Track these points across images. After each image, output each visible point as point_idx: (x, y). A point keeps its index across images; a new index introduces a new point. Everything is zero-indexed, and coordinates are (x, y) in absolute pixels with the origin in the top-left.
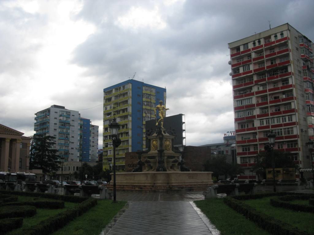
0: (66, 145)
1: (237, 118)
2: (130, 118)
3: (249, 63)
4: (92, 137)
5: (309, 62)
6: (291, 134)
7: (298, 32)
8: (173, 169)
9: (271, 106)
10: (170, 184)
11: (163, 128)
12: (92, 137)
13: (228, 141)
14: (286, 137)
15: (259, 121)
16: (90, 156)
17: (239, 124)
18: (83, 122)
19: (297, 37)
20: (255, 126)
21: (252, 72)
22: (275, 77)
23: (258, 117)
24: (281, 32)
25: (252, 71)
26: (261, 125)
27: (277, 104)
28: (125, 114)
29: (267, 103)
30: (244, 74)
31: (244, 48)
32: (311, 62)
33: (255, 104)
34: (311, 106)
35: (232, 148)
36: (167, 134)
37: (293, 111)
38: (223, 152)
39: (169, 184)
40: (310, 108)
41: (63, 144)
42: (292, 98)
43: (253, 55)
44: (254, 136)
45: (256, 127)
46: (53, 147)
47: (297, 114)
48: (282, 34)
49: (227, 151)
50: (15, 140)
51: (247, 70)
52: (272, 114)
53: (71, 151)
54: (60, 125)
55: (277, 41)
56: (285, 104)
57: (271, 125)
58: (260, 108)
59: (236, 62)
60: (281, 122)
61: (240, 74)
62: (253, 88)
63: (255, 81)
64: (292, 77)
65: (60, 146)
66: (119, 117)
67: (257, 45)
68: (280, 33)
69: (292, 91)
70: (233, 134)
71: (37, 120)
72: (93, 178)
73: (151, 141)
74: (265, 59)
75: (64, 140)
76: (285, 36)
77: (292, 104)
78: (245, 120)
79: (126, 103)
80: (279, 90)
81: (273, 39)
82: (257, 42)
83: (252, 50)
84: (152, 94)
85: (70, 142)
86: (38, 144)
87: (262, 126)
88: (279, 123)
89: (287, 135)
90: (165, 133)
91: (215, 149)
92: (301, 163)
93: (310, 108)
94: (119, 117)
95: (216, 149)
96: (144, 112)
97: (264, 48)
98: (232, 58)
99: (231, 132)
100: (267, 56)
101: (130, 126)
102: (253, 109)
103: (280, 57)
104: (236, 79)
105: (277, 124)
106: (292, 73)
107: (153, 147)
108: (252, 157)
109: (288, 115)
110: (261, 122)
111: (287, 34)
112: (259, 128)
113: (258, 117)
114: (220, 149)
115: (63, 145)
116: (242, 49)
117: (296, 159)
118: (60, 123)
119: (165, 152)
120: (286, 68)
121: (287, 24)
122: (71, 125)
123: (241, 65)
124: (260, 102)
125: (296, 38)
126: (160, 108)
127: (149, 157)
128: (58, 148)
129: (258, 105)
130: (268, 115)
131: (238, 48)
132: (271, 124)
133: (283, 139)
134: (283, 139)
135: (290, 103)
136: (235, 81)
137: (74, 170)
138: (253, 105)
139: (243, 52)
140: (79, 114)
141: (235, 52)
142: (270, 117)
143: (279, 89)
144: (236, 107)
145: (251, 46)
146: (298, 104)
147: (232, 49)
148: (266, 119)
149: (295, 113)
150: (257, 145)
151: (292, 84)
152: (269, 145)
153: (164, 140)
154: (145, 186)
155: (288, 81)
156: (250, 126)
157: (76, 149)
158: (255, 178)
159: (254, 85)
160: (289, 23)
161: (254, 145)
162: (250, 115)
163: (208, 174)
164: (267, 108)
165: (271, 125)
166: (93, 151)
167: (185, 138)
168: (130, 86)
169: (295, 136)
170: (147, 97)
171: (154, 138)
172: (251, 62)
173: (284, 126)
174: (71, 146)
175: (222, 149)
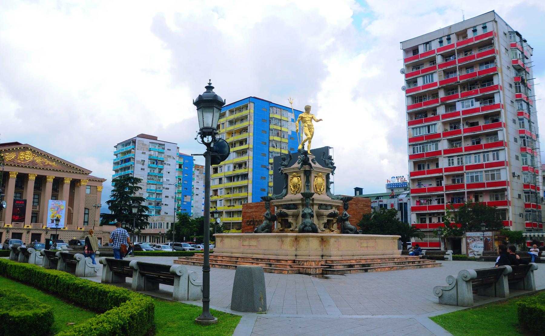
0: (157, 192)
1: (412, 154)
2: (251, 153)
3: (432, 72)
4: (195, 181)
5: (524, 72)
6: (496, 180)
7: (507, 25)
8: (329, 229)
9: (466, 138)
10: (328, 258)
11: (311, 154)
12: (195, 181)
13: (392, 190)
14: (489, 185)
15: (447, 160)
17: (415, 163)
18: (184, 161)
19: (506, 32)
20: (440, 167)
21: (437, 85)
22: (473, 92)
23: (444, 154)
24: (483, 24)
25: (436, 83)
27: (475, 133)
28: (244, 147)
29: (460, 132)
30: (424, 87)
32: (527, 72)
33: (440, 134)
34: (527, 138)
35: (400, 200)
36: (318, 165)
37: (501, 144)
38: (386, 205)
39: (325, 258)
40: (524, 140)
41: (153, 190)
42: (500, 125)
43: (439, 60)
44: (437, 182)
46: (137, 194)
47: (506, 148)
48: (485, 28)
49: (392, 205)
50: (79, 181)
51: (429, 81)
52: (467, 149)
53: (164, 201)
54: (150, 163)
55: (477, 38)
56: (488, 135)
57: (466, 166)
59: (410, 71)
60: (482, 162)
61: (419, 89)
62: (437, 108)
63: (441, 99)
64: (499, 92)
65: (149, 192)
66: (234, 152)
67: (445, 43)
68: (482, 26)
69: (498, 114)
70: (399, 180)
71: (116, 155)
72: (195, 240)
73: (290, 177)
74: (458, 65)
75: (156, 184)
76: (489, 30)
77: (499, 133)
78: (425, 158)
79: (244, 131)
80: (479, 111)
81: (470, 35)
82: (445, 39)
83: (437, 52)
84: (283, 118)
85: (164, 188)
87: (451, 166)
88: (477, 163)
89: (490, 181)
90: (315, 163)
91: (374, 202)
92: (511, 225)
93: (524, 140)
95: (376, 202)
96: (271, 145)
97: (456, 48)
98: (406, 63)
99: (397, 177)
100: (460, 61)
101: (250, 165)
102: (438, 141)
103: (481, 63)
104: (412, 96)
105: (476, 164)
106: (499, 87)
107: (292, 187)
108: (434, 214)
109: (493, 151)
110: (449, 160)
111: (493, 26)
112: (447, 170)
113: (444, 154)
114: (382, 201)
115: (154, 192)
116: (421, 50)
117: (504, 218)
118: (150, 161)
119: (315, 196)
120: (490, 79)
121: (493, 11)
122: (165, 164)
123: (420, 75)
124: (449, 130)
125: (505, 34)
126: (307, 119)
127: (288, 207)
128: (146, 195)
129: (445, 134)
130: (460, 150)
131: (415, 50)
132: (465, 165)
134: (484, 187)
135: (496, 133)
136: (410, 99)
137: (167, 228)
138: (438, 135)
139: (422, 55)
140: (178, 148)
141: (411, 55)
142: (464, 153)
144: (411, 137)
145: (435, 46)
146: (508, 133)
147: (406, 51)
148: (458, 156)
149: (503, 148)
150: (442, 195)
151: (499, 103)
152: (291, 229)
153: (313, 175)
154: (278, 260)
155: (493, 99)
156: (433, 167)
158: (440, 246)
159: (440, 105)
160: (495, 11)
161: (439, 196)
163: (393, 238)
164: (460, 139)
165: (466, 166)
166: (197, 202)
167: (333, 183)
168: (251, 109)
169: (504, 183)
170: (276, 123)
171: (295, 172)
172: (436, 70)
173: (486, 168)
174: (165, 193)
175: (385, 201)
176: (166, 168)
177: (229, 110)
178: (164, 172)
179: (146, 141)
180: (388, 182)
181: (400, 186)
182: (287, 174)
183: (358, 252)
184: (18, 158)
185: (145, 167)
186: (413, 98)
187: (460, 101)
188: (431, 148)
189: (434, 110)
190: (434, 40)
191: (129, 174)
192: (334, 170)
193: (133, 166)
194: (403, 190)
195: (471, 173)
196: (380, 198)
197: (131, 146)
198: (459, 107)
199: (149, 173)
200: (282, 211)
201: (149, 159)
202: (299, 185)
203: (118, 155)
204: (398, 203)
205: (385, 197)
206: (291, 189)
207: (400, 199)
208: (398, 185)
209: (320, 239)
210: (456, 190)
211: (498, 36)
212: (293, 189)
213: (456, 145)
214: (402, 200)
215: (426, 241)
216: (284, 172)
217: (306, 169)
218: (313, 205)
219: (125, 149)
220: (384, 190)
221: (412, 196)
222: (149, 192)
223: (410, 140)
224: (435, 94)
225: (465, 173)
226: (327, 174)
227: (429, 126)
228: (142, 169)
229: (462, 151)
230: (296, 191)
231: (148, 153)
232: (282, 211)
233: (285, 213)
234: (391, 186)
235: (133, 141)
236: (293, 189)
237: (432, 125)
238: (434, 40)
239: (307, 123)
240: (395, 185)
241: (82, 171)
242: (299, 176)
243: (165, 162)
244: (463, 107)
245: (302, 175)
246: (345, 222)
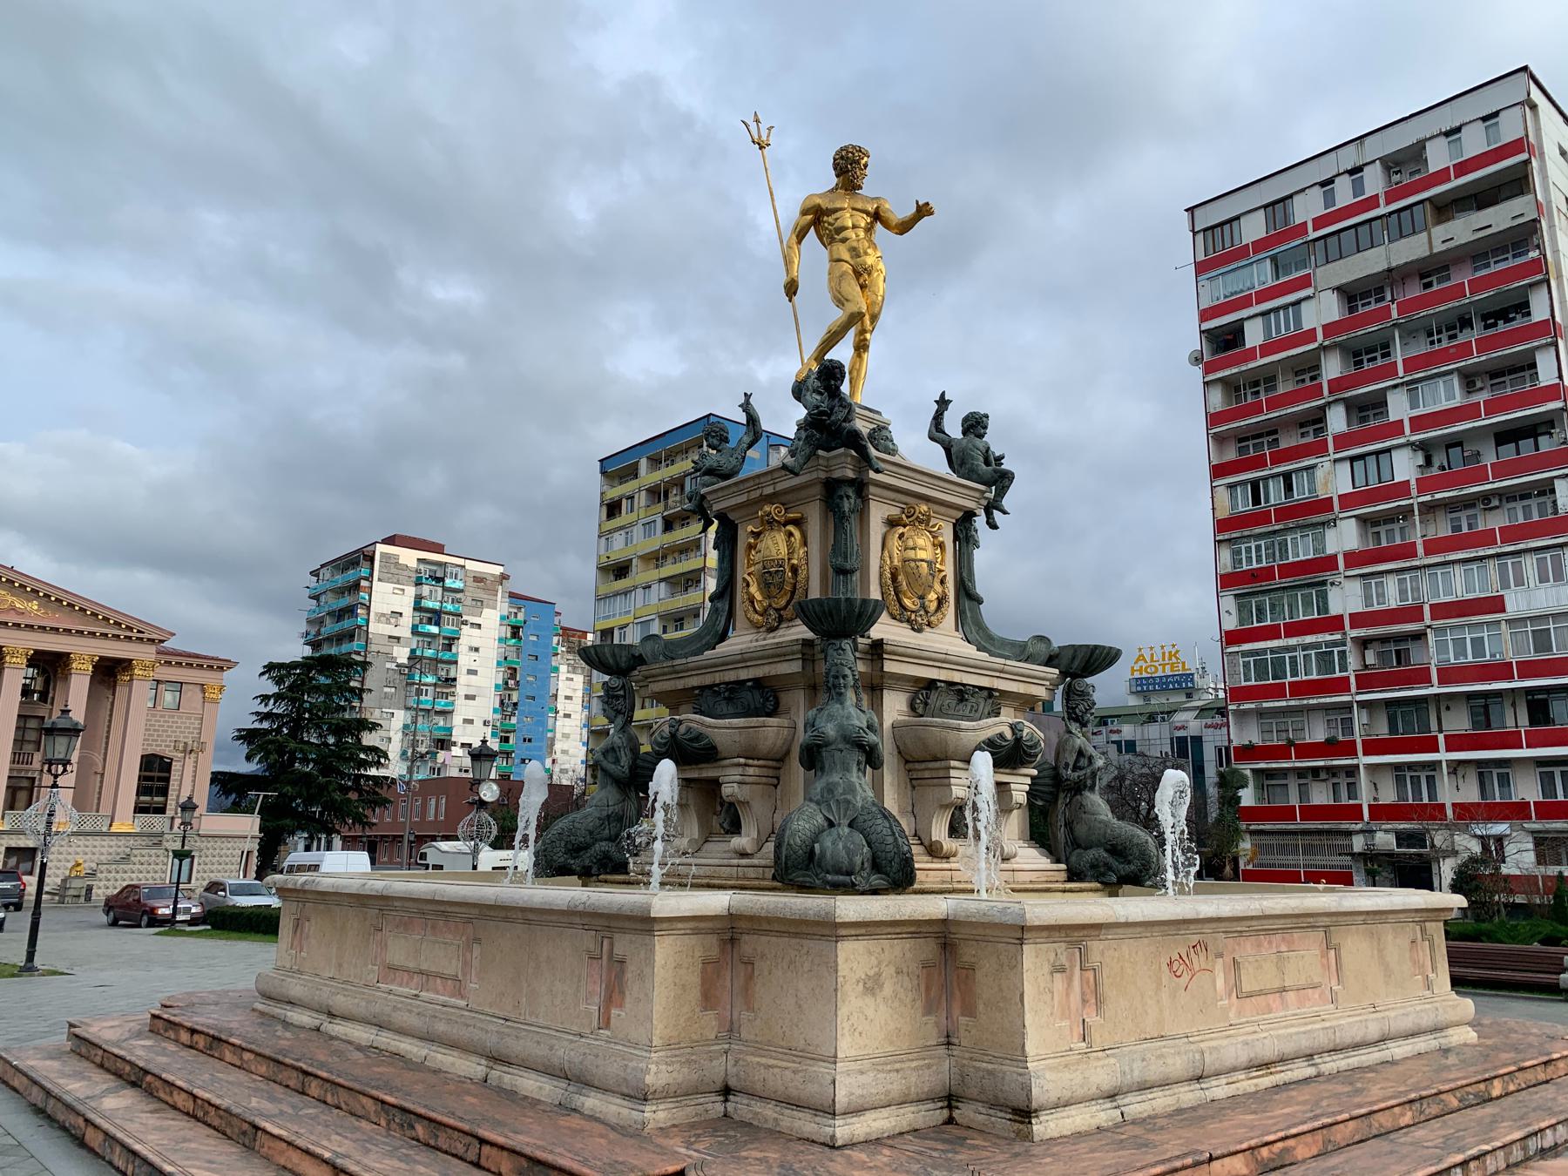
14: (1528, 669)
16: (418, 653)
23: (1348, 566)
26: (1368, 602)
30: (1267, 349)
31: (1271, 222)
45: (1341, 617)
52: (1432, 547)
55: (1462, 168)
58: (1363, 520)
66: (661, 580)
71: (316, 597)
86: (1244, 803)
87: (1376, 607)
89: (1532, 656)
94: (661, 580)
102: (1323, 524)
107: (753, 589)
108: (1315, 771)
110: (1367, 587)
112: (1358, 620)
113: (1348, 566)
114: (1119, 732)
121: (1525, 69)
122: (465, 623)
130: (1408, 551)
133: (1509, 677)
134: (1510, 677)
138: (1326, 505)
143: (1478, 416)
157: (485, 723)
162: (1259, 560)
164: (1407, 512)
171: (770, 499)
176: (468, 636)
177: (648, 458)
178: (462, 648)
180: (1132, 674)
181: (1171, 686)
182: (731, 516)
183: (1233, 1050)
186: (1231, 387)
187: (1402, 384)
188: (1301, 549)
189: (1317, 420)
190: (1303, 190)
191: (350, 653)
192: (1001, 493)
193: (365, 628)
194: (1184, 699)
195: (1452, 628)
196: (1112, 722)
198: (1399, 408)
200: (682, 729)
201: (414, 609)
202: (794, 570)
203: (323, 598)
204: (1172, 739)
205: (1126, 718)
206: (752, 600)
207: (1179, 725)
208: (1167, 684)
209: (929, 948)
210: (1413, 689)
211: (1542, 154)
212: (758, 596)
213: (1391, 537)
214: (1183, 728)
215: (1295, 866)
216: (716, 507)
217: (837, 474)
218: (875, 687)
219: (341, 579)
221: (1237, 713)
223: (1222, 525)
224: (1308, 367)
225: (1429, 630)
226: (960, 514)
227: (1287, 477)
229: (1414, 555)
230: (777, 610)
232: (682, 729)
233: (699, 737)
234: (1142, 685)
236: (758, 596)
237: (1297, 471)
238: (1303, 190)
239: (844, 240)
240: (1154, 684)
241: (139, 632)
242: (798, 523)
243: (465, 618)
244: (1414, 405)
245: (814, 514)
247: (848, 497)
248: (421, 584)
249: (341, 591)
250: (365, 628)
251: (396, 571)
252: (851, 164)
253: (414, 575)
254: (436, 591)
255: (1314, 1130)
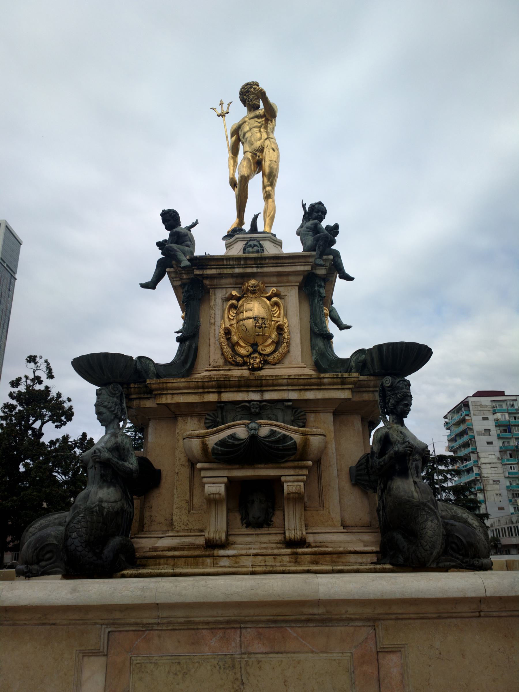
118: (498, 428)
179: (486, 401)
184: (119, 405)
185: (493, 437)
197: (464, 412)
199: (501, 448)
201: (496, 426)
219: (457, 417)
220: (299, 237)
222: (508, 477)
228: (488, 443)
231: (492, 417)
235: (465, 404)
246: (275, 344)
247: (86, 497)
248: (496, 413)
249: (458, 424)
250: (473, 440)
251: (482, 409)
252: (245, 95)
253: (491, 409)
254: (505, 415)
255: (266, 616)
